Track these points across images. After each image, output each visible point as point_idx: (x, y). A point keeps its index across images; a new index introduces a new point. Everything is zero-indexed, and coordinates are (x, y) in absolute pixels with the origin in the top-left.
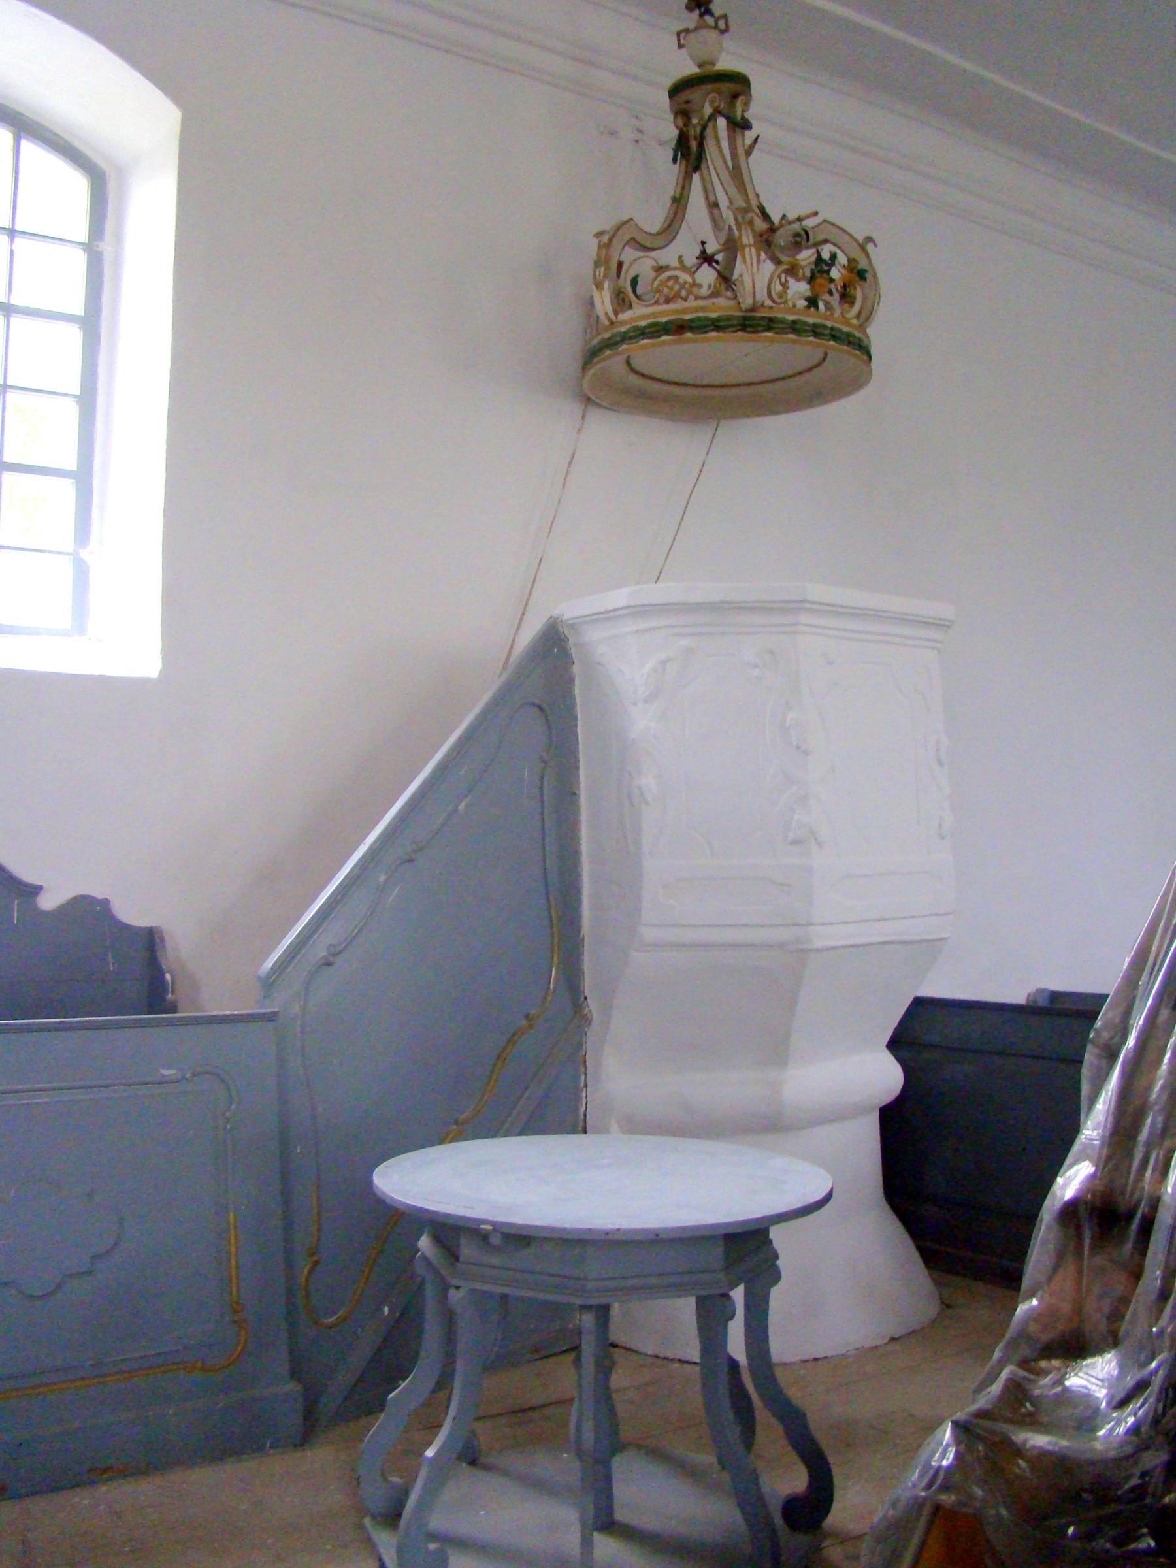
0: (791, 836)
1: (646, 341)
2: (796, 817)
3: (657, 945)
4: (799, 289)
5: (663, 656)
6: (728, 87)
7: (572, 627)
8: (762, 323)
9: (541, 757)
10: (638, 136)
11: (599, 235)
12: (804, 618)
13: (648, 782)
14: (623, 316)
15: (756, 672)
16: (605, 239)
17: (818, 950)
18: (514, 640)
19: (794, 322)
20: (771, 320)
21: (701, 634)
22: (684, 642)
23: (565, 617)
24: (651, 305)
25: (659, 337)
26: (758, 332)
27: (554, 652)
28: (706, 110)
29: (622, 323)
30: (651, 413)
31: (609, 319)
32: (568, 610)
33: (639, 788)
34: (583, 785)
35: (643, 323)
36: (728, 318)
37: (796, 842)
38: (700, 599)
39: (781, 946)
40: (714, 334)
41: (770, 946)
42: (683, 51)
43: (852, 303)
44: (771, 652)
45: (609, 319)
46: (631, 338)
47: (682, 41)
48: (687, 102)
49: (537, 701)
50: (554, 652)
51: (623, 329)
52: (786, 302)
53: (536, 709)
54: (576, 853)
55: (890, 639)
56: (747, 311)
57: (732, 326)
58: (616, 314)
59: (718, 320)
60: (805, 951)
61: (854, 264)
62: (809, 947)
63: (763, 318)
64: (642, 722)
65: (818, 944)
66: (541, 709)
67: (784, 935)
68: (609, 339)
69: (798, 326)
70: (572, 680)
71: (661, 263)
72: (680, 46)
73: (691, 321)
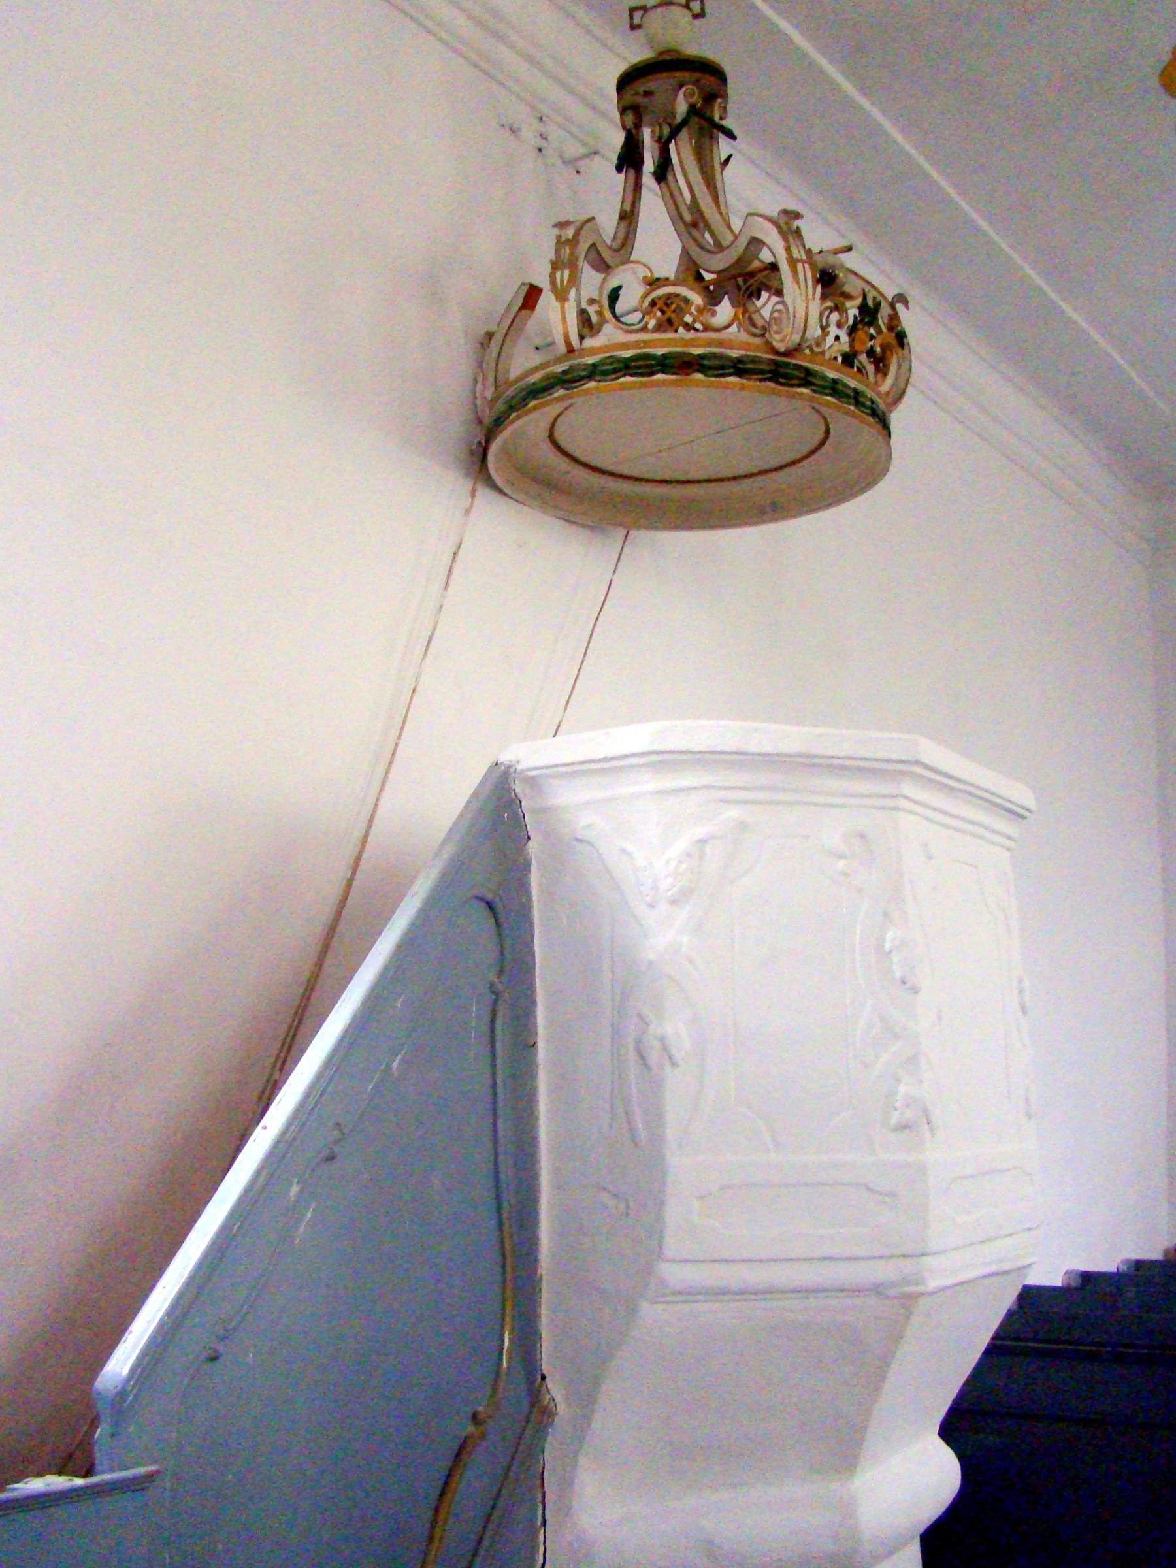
0: (895, 1118)
1: (628, 379)
2: (902, 1089)
3: (688, 1293)
4: (837, 341)
5: (699, 832)
6: (709, 81)
7: (532, 782)
8: (796, 373)
9: (492, 985)
10: (543, 144)
11: (562, 225)
12: (908, 788)
13: (674, 1027)
14: (589, 343)
15: (841, 864)
16: (570, 233)
17: (931, 1294)
18: (376, 805)
19: (835, 381)
20: (808, 372)
21: (759, 803)
22: (733, 813)
23: (519, 767)
24: (637, 331)
25: (652, 374)
26: (792, 386)
27: (502, 818)
28: (673, 104)
29: (593, 351)
30: (544, 505)
31: (568, 343)
32: (527, 755)
33: (662, 1039)
34: (541, 1031)
35: (627, 354)
36: (754, 360)
37: (903, 1127)
38: (768, 748)
39: (877, 1289)
40: (733, 379)
41: (858, 1291)
42: (639, 33)
43: (885, 374)
44: (862, 836)
45: (568, 343)
46: (605, 373)
47: (636, 21)
48: (648, 94)
49: (489, 896)
50: (502, 818)
51: (590, 360)
52: (823, 353)
53: (484, 905)
54: (534, 1141)
55: (970, 827)
56: (894, 317)
57: (761, 372)
58: (582, 338)
59: (740, 360)
60: (913, 1297)
61: (895, 322)
62: (921, 1289)
63: (798, 367)
64: (664, 938)
65: (933, 1284)
66: (490, 905)
67: (882, 1272)
68: (564, 372)
69: (840, 387)
70: (526, 867)
71: (656, 275)
72: (633, 27)
73: (702, 357)
